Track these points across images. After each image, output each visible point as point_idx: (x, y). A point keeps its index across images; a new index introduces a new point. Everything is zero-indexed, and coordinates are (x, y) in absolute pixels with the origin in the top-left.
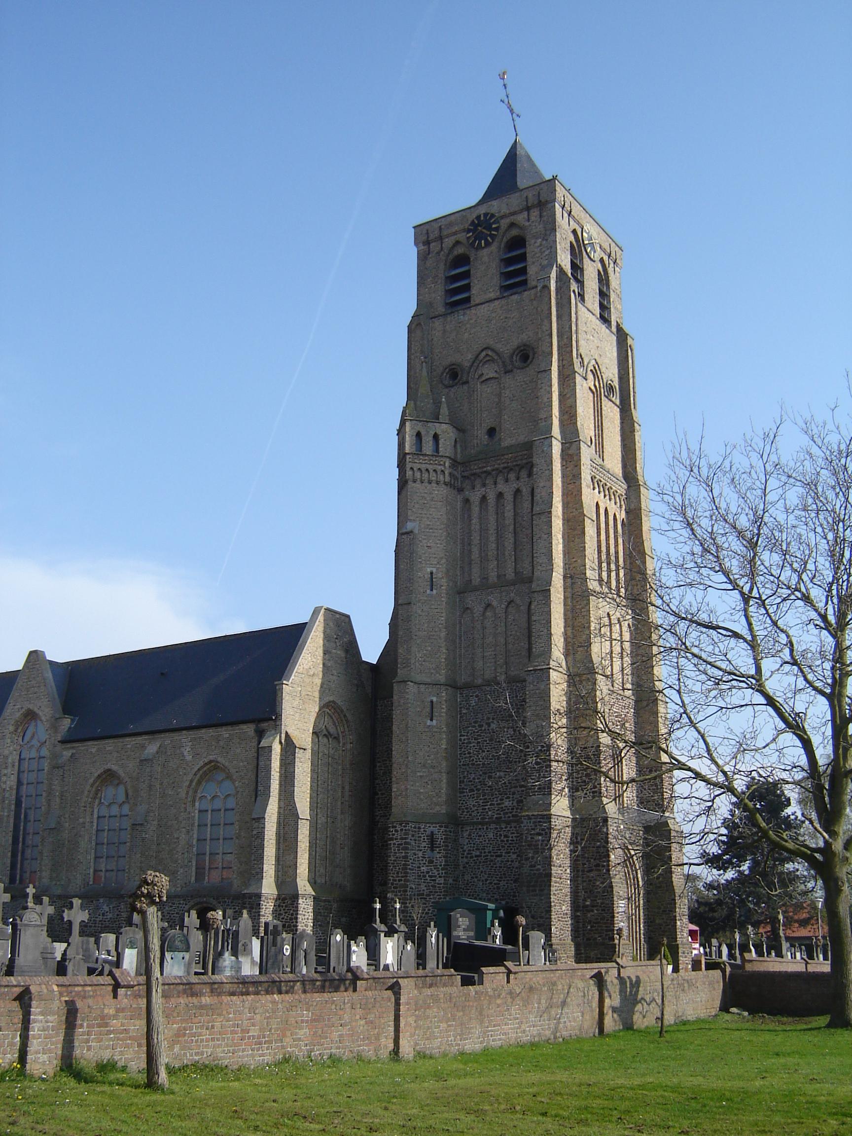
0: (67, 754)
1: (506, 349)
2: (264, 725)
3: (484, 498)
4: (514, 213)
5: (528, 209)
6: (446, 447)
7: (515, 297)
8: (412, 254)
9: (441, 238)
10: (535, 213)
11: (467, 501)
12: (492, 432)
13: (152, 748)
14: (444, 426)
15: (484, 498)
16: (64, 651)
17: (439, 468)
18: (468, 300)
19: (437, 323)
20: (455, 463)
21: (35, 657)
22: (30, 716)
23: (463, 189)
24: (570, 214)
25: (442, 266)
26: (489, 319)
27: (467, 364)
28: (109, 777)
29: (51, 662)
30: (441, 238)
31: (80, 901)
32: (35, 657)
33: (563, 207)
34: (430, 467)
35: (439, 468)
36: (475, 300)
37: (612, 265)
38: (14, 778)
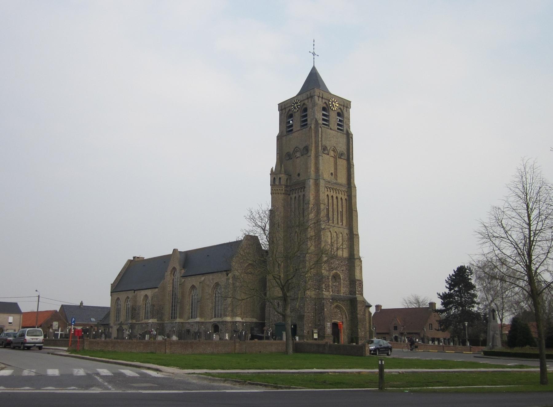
0: (183, 280)
1: (302, 147)
2: (228, 272)
3: (295, 197)
4: (304, 100)
5: (308, 98)
6: (283, 182)
7: (304, 130)
8: (278, 113)
9: (285, 108)
10: (310, 100)
11: (291, 198)
12: (299, 175)
13: (203, 278)
14: (283, 175)
15: (295, 197)
16: (183, 248)
17: (281, 189)
18: (292, 130)
19: (284, 138)
20: (286, 186)
21: (175, 251)
22: (174, 269)
23: (292, 89)
24: (322, 98)
25: (285, 118)
26: (296, 139)
27: (292, 152)
28: (193, 287)
29: (180, 252)
30: (285, 108)
31: (437, 308)
32: (175, 251)
33: (319, 97)
34: (278, 189)
35: (281, 189)
36: (294, 130)
37: (345, 108)
38: (171, 288)
